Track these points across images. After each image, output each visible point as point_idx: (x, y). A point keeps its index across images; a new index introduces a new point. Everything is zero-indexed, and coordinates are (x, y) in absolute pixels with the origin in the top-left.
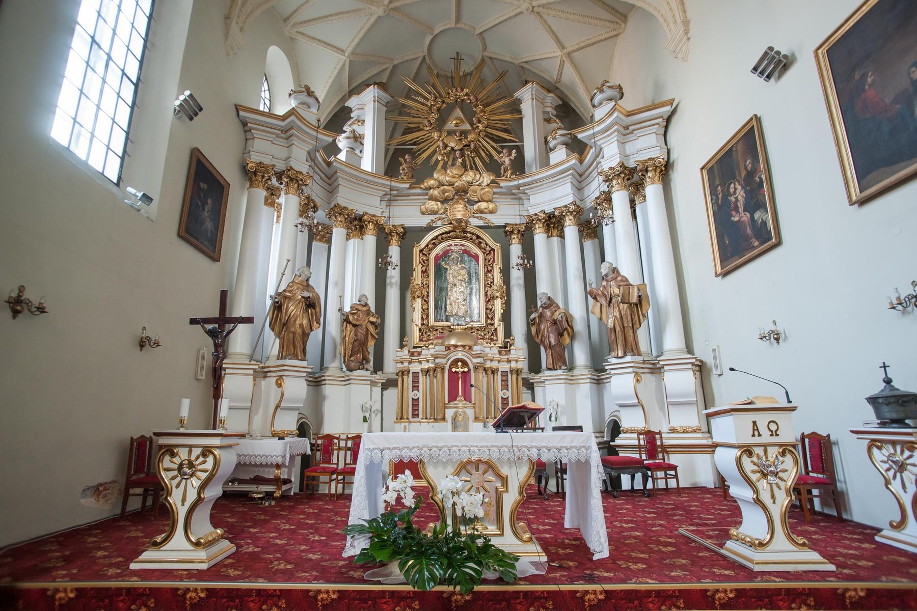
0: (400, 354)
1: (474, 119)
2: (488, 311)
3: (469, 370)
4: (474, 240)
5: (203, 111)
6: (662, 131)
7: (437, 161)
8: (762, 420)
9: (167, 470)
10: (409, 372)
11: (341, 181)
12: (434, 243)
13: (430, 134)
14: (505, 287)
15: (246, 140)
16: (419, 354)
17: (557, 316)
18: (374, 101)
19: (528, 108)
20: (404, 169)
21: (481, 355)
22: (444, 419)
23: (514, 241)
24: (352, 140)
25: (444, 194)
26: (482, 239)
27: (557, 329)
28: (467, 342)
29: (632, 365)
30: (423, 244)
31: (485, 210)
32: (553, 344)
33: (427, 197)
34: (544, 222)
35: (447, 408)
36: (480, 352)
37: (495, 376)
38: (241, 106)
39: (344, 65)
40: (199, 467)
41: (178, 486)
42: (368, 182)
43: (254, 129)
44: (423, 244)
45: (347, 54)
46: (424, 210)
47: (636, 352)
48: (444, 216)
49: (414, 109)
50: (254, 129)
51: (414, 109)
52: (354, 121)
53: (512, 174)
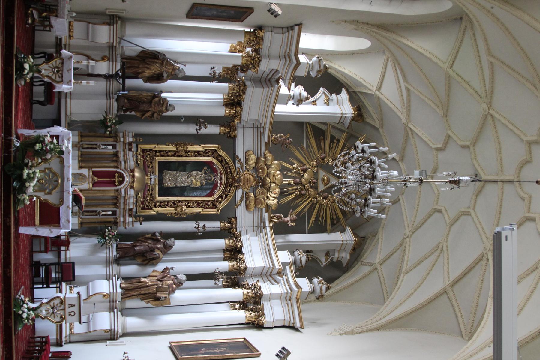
0: (130, 134)
1: (326, 194)
2: (166, 203)
3: (116, 186)
4: (224, 193)
5: (274, 18)
6: (286, 324)
7: (292, 164)
8: (75, 309)
9: (56, 61)
10: (116, 142)
11: (266, 90)
12: (222, 161)
13: (315, 158)
14: (185, 216)
15: (282, 28)
16: (130, 150)
17: (157, 253)
18: (342, 113)
19: (336, 237)
20: (281, 137)
21: (127, 194)
22: (81, 167)
23: (223, 224)
24: (299, 98)
25: (261, 169)
26: (225, 199)
27: (147, 252)
28: (136, 185)
29: (115, 291)
30: (222, 153)
31: (248, 201)
32: (136, 249)
33: (259, 155)
34: (234, 246)
35: (89, 170)
36: (129, 193)
37: (112, 206)
38: (301, 27)
39: (371, 90)
40: (57, 75)
41: (50, 67)
42: (268, 110)
43: (289, 34)
44: (222, 153)
45: (377, 92)
46: (249, 153)
47: (124, 296)
48: (244, 169)
49: (337, 145)
50: (289, 34)
51: (337, 145)
52: (328, 96)
53: (275, 222)
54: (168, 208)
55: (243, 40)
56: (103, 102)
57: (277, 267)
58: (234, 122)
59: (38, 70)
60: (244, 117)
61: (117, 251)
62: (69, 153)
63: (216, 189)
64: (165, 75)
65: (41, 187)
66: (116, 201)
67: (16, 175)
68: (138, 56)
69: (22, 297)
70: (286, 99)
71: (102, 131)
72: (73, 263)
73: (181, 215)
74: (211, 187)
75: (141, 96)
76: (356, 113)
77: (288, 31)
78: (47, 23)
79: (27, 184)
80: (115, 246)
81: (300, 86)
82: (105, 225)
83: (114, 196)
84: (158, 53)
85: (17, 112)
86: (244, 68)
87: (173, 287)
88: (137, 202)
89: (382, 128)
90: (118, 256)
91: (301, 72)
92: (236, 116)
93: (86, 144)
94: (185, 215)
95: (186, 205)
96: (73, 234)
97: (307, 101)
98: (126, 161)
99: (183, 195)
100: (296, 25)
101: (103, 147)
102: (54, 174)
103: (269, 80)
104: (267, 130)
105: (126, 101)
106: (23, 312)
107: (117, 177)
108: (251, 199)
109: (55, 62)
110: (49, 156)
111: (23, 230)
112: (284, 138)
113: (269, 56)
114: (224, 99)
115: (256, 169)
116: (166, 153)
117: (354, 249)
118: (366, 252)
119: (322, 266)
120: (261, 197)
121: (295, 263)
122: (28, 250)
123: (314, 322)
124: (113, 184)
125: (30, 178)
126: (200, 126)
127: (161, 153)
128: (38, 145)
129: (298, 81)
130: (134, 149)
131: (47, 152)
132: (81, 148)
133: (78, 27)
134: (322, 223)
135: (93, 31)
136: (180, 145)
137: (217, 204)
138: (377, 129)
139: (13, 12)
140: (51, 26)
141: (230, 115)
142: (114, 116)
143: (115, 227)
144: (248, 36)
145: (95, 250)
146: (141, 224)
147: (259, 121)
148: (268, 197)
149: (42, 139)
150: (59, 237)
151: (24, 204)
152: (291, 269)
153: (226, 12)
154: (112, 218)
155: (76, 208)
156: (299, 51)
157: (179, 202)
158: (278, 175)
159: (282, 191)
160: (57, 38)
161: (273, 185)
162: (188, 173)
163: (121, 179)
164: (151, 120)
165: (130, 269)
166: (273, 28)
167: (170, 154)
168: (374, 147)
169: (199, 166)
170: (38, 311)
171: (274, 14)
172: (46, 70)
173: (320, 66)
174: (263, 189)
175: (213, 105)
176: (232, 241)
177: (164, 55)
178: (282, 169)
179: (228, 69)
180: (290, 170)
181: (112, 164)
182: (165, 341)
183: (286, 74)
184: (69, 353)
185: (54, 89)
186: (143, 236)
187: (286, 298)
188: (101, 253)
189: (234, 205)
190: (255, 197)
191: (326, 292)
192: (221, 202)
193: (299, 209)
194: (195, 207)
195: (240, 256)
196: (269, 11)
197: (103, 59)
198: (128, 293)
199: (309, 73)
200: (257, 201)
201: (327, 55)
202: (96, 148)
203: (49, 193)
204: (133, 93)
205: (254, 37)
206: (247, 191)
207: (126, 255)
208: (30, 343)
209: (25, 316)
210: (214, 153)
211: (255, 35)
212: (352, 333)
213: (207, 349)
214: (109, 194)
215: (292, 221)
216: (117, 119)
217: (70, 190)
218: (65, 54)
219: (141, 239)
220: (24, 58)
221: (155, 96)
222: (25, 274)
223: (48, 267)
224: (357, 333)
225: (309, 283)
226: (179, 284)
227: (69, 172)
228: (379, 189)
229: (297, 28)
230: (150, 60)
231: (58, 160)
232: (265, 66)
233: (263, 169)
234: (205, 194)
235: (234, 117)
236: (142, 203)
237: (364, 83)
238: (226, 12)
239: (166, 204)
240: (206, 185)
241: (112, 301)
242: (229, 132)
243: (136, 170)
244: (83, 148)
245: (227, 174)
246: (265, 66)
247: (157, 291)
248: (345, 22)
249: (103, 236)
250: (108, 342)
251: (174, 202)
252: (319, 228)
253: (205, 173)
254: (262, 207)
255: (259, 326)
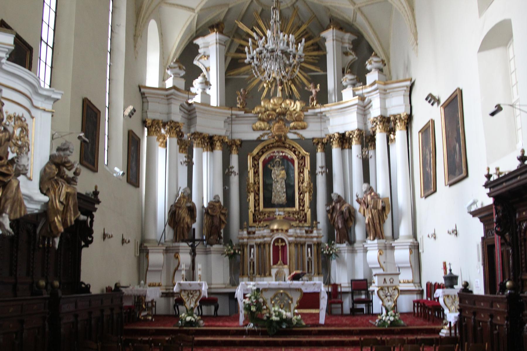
0: (241, 233)
3: (286, 245)
7: (264, 88)
8: (388, 278)
10: (247, 245)
11: (197, 114)
12: (262, 152)
14: (312, 184)
15: (143, 102)
16: (254, 233)
17: (344, 209)
19: (330, 46)
20: (239, 99)
22: (270, 275)
23: (319, 150)
24: (204, 84)
27: (343, 217)
28: (285, 228)
30: (255, 152)
37: (304, 249)
41: (188, 300)
44: (255, 152)
45: (196, 11)
48: (269, 132)
53: (317, 103)
54: (305, 199)
55: (155, 138)
56: (213, 257)
57: (357, 101)
58: (227, 142)
59: (191, 310)
60: (222, 133)
61: (342, 243)
62: (258, 284)
63: (287, 157)
64: (189, 204)
65: (287, 307)
66: (299, 245)
67: (277, 326)
68: (173, 228)
69: (377, 321)
70: (205, 96)
71: (238, 257)
72: (352, 281)
73: (311, 188)
74: (285, 161)
75: (207, 224)
76: (215, 30)
77: (146, 97)
78: (150, 305)
79: (284, 317)
80: (338, 245)
81: (194, 83)
82: (513, 87)
83: (295, 246)
84: (170, 211)
85: (225, 326)
86: (180, 135)
87: (374, 195)
88: (299, 227)
89: (228, 5)
90: (347, 242)
91: (181, 84)
92: (222, 140)
93: (249, 271)
94: (311, 184)
95: (302, 183)
96: (327, 281)
97: (207, 76)
98: (264, 237)
99: (293, 186)
100: (140, 90)
101: (252, 256)
102: (275, 296)
103: (189, 111)
104: (234, 112)
105: (212, 237)
106: (389, 320)
107: (278, 245)
108: (297, 125)
109: (184, 296)
110: (261, 300)
111: (322, 321)
112: (240, 97)
113: (169, 113)
114: (207, 151)
115: (269, 121)
116: (257, 202)
117: (341, 29)
118: (343, 17)
119: (357, 58)
120: (294, 117)
121: (354, 85)
122: (340, 318)
123: (407, 68)
124: (284, 248)
125: (279, 315)
126: (232, 172)
127: (256, 206)
128: (252, 309)
129: (189, 85)
130: (253, 229)
131: (257, 302)
132: (253, 275)
133: (151, 278)
134: (317, 60)
135: (154, 266)
136: (249, 189)
137: (300, 155)
138: (229, 10)
139: (146, 330)
140: (152, 301)
141: (221, 145)
142: (225, 247)
143: (322, 246)
144: (152, 133)
145: (342, 262)
146: (319, 223)
147: (226, 120)
148: (294, 110)
149: (247, 306)
150: (328, 293)
151: (301, 319)
152: (358, 90)
153: (132, 154)
154: (314, 248)
155: (305, 278)
156: (161, 86)
157: (299, 189)
158: (274, 102)
159: (289, 97)
160: (162, 296)
161: (283, 105)
162: (273, 182)
163: (280, 241)
164: (227, 215)
165: (359, 232)
166: (144, 111)
167: (257, 198)
168: (249, 48)
169: (267, 173)
170: (389, 308)
171: (133, 112)
172: (191, 303)
173: (175, 68)
174: (287, 115)
175: (213, 160)
176: (334, 142)
177: (172, 206)
178: (268, 97)
179: (180, 148)
180: (269, 90)
181: (267, 248)
182: (420, 202)
183: (183, 97)
184: (428, 284)
185: (205, 297)
186: (330, 221)
187: (384, 94)
188: (344, 257)
189: (302, 141)
190: (294, 121)
191: (378, 57)
192: (299, 152)
193: (305, 81)
194: (304, 175)
195: (347, 134)
196: (130, 117)
197: (177, 258)
198: (378, 235)
199: (182, 77)
200: (298, 119)
201: (164, 58)
202: (254, 263)
203: (292, 300)
204: (205, 231)
205: (153, 127)
206: (289, 129)
207: (347, 235)
208: (418, 316)
209: (392, 319)
210: (254, 159)
211: (150, 127)
212: (416, 34)
213: (427, 166)
214: (293, 251)
215: (315, 87)
216: (228, 245)
217: (288, 283)
218: (176, 289)
219: (332, 223)
220: (182, 321)
221: (207, 213)
222: (359, 319)
223: (354, 302)
224: (416, 29)
225: (371, 73)
226: (370, 190)
227: (274, 284)
228: (282, 46)
229: (142, 90)
230: (176, 217)
231: (264, 293)
232: (178, 117)
233: (269, 115)
234: (292, 166)
235: (223, 142)
236: (300, 222)
237: (188, 24)
238: (132, 154)
239: (301, 200)
240: (284, 166)
241: (385, 247)
242: (237, 146)
243: (272, 227)
244: (254, 273)
245: (274, 147)
246: (178, 117)
247: (376, 208)
248: (135, 47)
249: (330, 255)
250: (420, 251)
251: (300, 194)
252: (322, 62)
253: (273, 166)
254: (303, 115)
255: (410, 118)
